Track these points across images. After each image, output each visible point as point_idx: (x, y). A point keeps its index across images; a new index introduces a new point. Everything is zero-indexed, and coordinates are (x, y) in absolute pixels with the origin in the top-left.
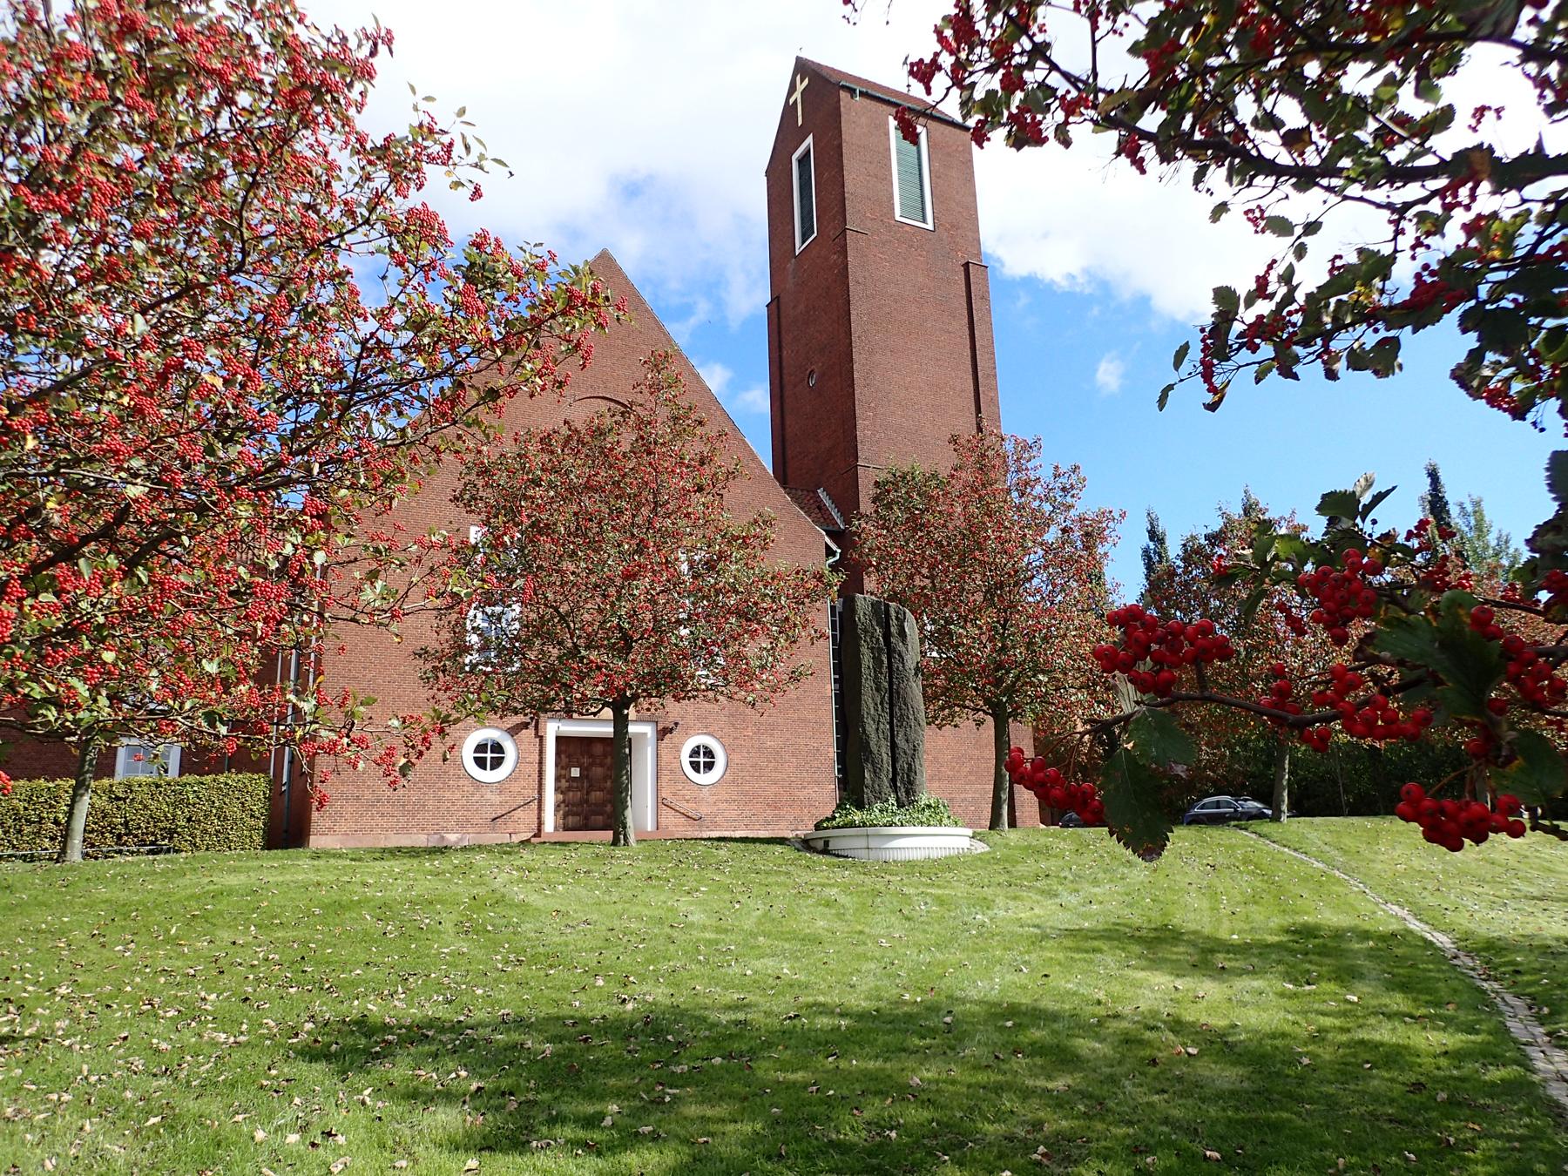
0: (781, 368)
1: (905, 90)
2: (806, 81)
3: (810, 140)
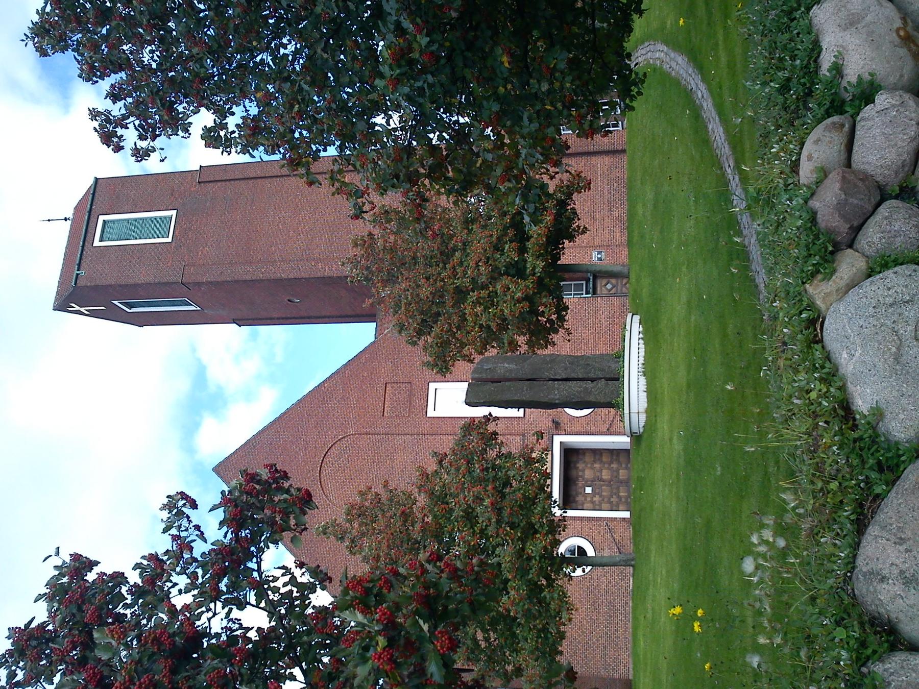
0: (287, 318)
1: (69, 222)
2: (73, 305)
3: (116, 302)
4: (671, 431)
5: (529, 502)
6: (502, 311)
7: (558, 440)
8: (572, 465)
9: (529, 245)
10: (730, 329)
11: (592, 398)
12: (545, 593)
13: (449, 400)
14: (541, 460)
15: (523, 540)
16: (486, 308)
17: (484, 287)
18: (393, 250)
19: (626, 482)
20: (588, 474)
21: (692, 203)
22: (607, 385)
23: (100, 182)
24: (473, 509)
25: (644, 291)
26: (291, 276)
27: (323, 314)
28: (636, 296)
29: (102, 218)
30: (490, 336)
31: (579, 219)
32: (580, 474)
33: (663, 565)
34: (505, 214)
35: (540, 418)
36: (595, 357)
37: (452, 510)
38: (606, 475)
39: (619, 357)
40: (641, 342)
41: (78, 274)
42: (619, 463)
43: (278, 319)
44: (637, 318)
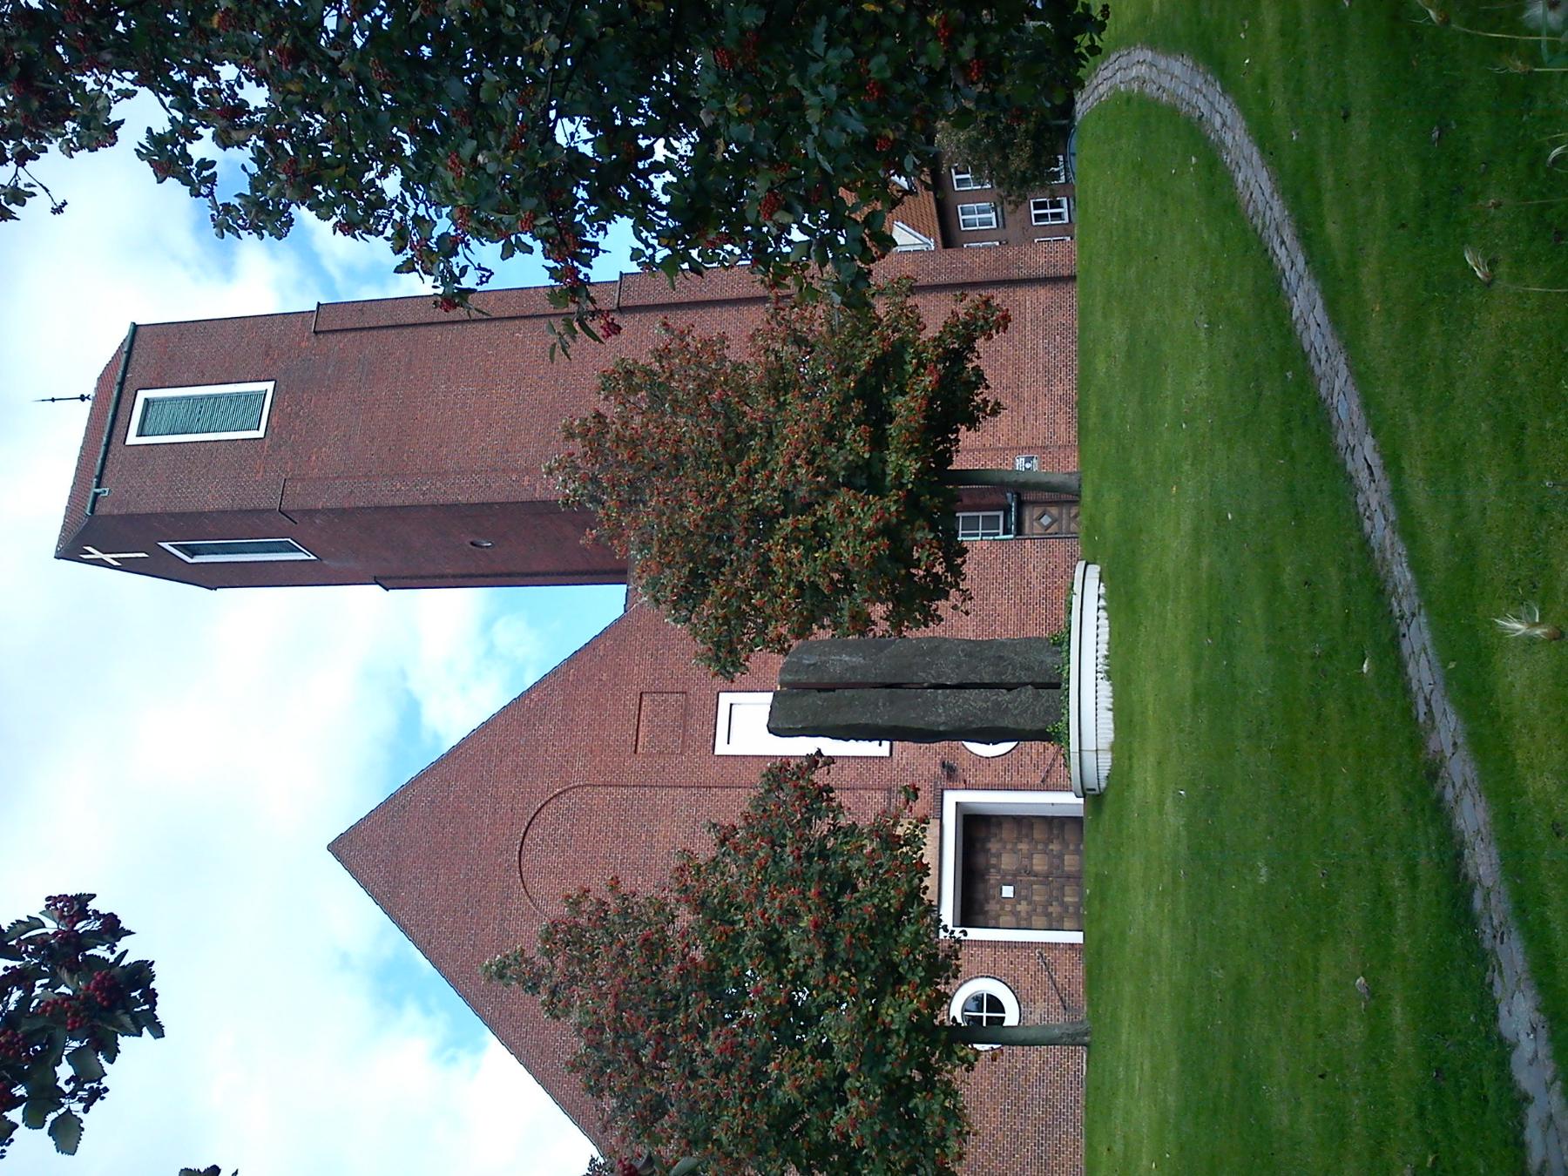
0: (471, 576)
1: (88, 403)
3: (165, 545)
4: (1161, 789)
5: (887, 923)
6: (839, 554)
7: (951, 798)
8: (978, 846)
9: (892, 429)
10: (1288, 576)
11: (1007, 722)
12: (917, 1101)
13: (746, 725)
14: (913, 841)
15: (877, 993)
16: (810, 550)
17: (807, 507)
18: (634, 444)
19: (1076, 878)
20: (1007, 862)
21: (1202, 335)
22: (1037, 697)
23: (141, 330)
24: (780, 937)
25: (1107, 518)
26: (475, 499)
27: (535, 568)
28: (1094, 527)
29: (142, 395)
30: (816, 604)
31: (987, 387)
32: (993, 861)
33: (1145, 1059)
34: (846, 373)
35: (919, 759)
36: (1012, 643)
37: (742, 934)
38: (1039, 864)
39: (1060, 643)
40: (1103, 614)
41: (96, 495)
42: (1065, 843)
43: (454, 576)
44: (1094, 571)
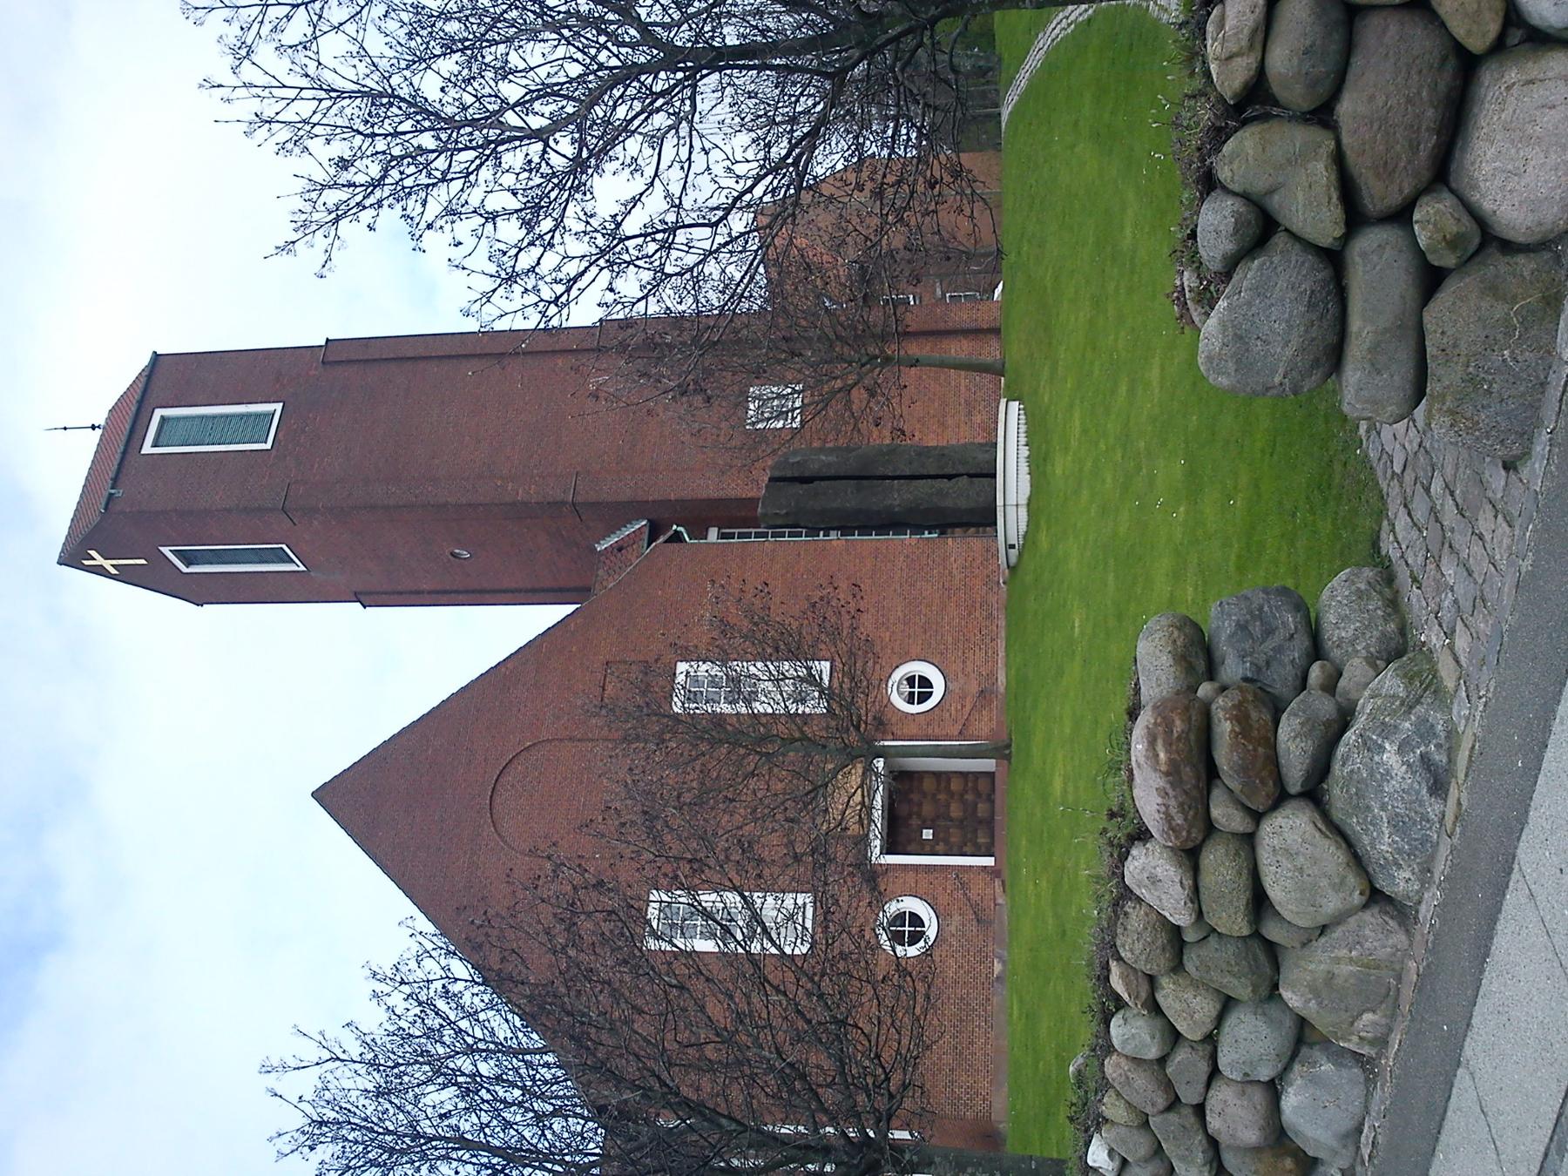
1: (99, 432)
2: (93, 553)
3: (166, 550)
29: (159, 413)
